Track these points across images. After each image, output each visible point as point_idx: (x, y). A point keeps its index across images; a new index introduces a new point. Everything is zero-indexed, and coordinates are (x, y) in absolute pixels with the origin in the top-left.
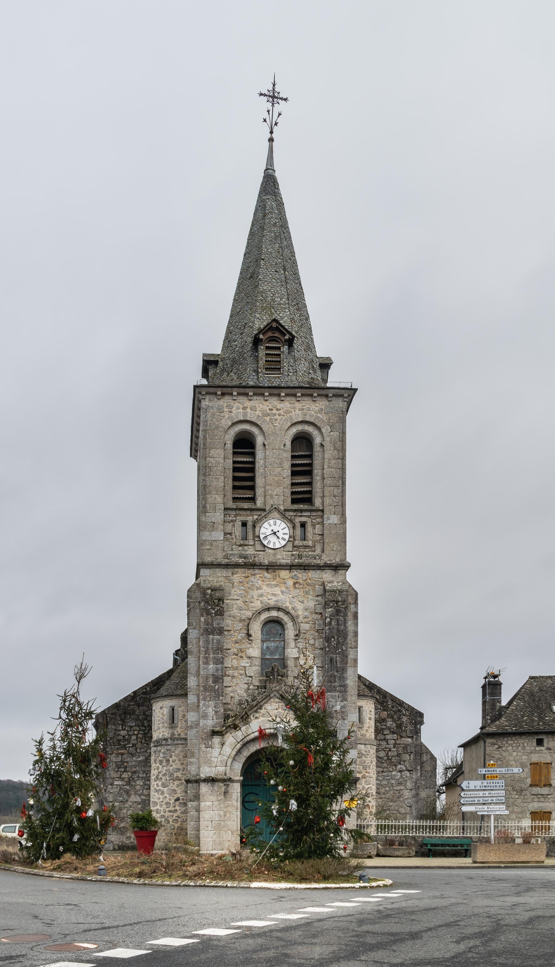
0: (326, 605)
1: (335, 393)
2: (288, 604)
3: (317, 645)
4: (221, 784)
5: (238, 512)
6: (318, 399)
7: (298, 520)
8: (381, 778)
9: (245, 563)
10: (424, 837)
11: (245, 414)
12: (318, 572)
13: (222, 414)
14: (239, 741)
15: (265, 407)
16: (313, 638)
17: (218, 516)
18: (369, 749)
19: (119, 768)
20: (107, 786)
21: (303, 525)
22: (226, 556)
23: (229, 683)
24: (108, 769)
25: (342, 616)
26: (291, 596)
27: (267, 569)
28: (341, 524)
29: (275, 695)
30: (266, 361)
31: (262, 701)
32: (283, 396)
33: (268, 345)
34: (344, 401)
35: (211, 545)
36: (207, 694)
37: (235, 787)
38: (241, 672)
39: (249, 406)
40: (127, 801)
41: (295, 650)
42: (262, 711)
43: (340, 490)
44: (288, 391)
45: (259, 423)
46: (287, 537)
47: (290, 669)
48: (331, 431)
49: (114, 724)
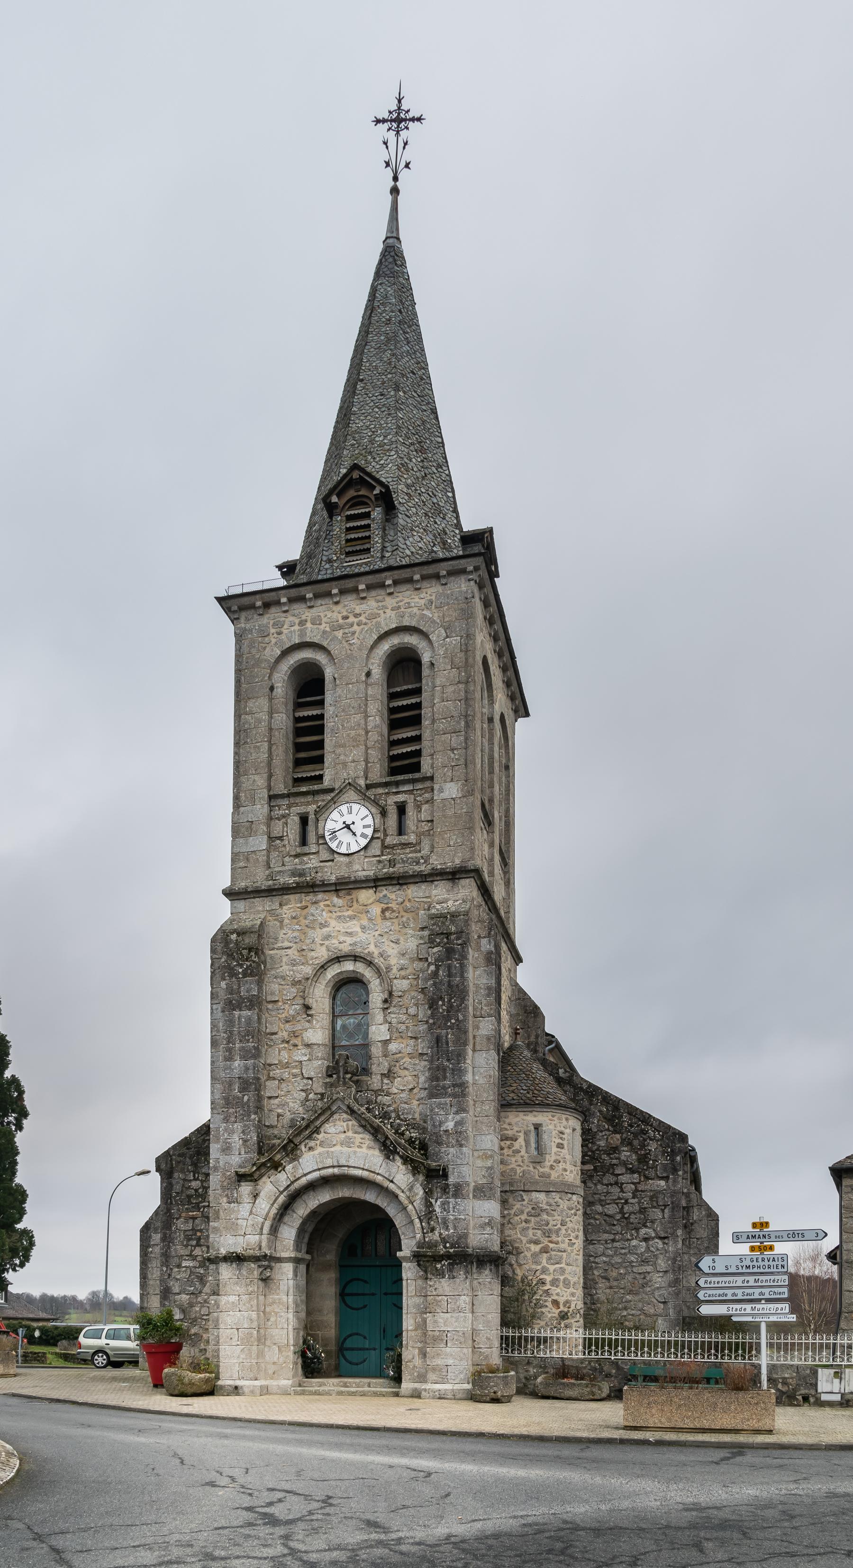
0: (431, 942)
1: (451, 568)
2: (372, 948)
3: (421, 1016)
4: (253, 1265)
5: (292, 800)
6: (425, 584)
7: (392, 800)
8: (610, 1252)
9: (297, 883)
10: (634, 1363)
11: (302, 633)
12: (423, 886)
13: (266, 639)
14: (282, 1189)
15: (335, 615)
16: (415, 1005)
17: (260, 810)
18: (557, 1199)
19: (189, 1240)
20: (171, 1269)
21: (401, 809)
22: (270, 877)
23: (275, 1091)
24: (173, 1243)
25: (456, 960)
26: (377, 933)
27: (337, 890)
28: (464, 797)
29: (339, 1108)
30: (347, 541)
31: (317, 1118)
32: (363, 590)
33: (349, 513)
34: (469, 580)
35: (248, 859)
36: (231, 1110)
37: (285, 1270)
38: (294, 1071)
39: (309, 619)
40: (200, 1292)
41: (384, 1028)
42: (320, 1137)
43: (462, 738)
44: (370, 579)
45: (325, 644)
46: (369, 832)
47: (375, 1060)
48: (447, 637)
49: (182, 1171)
